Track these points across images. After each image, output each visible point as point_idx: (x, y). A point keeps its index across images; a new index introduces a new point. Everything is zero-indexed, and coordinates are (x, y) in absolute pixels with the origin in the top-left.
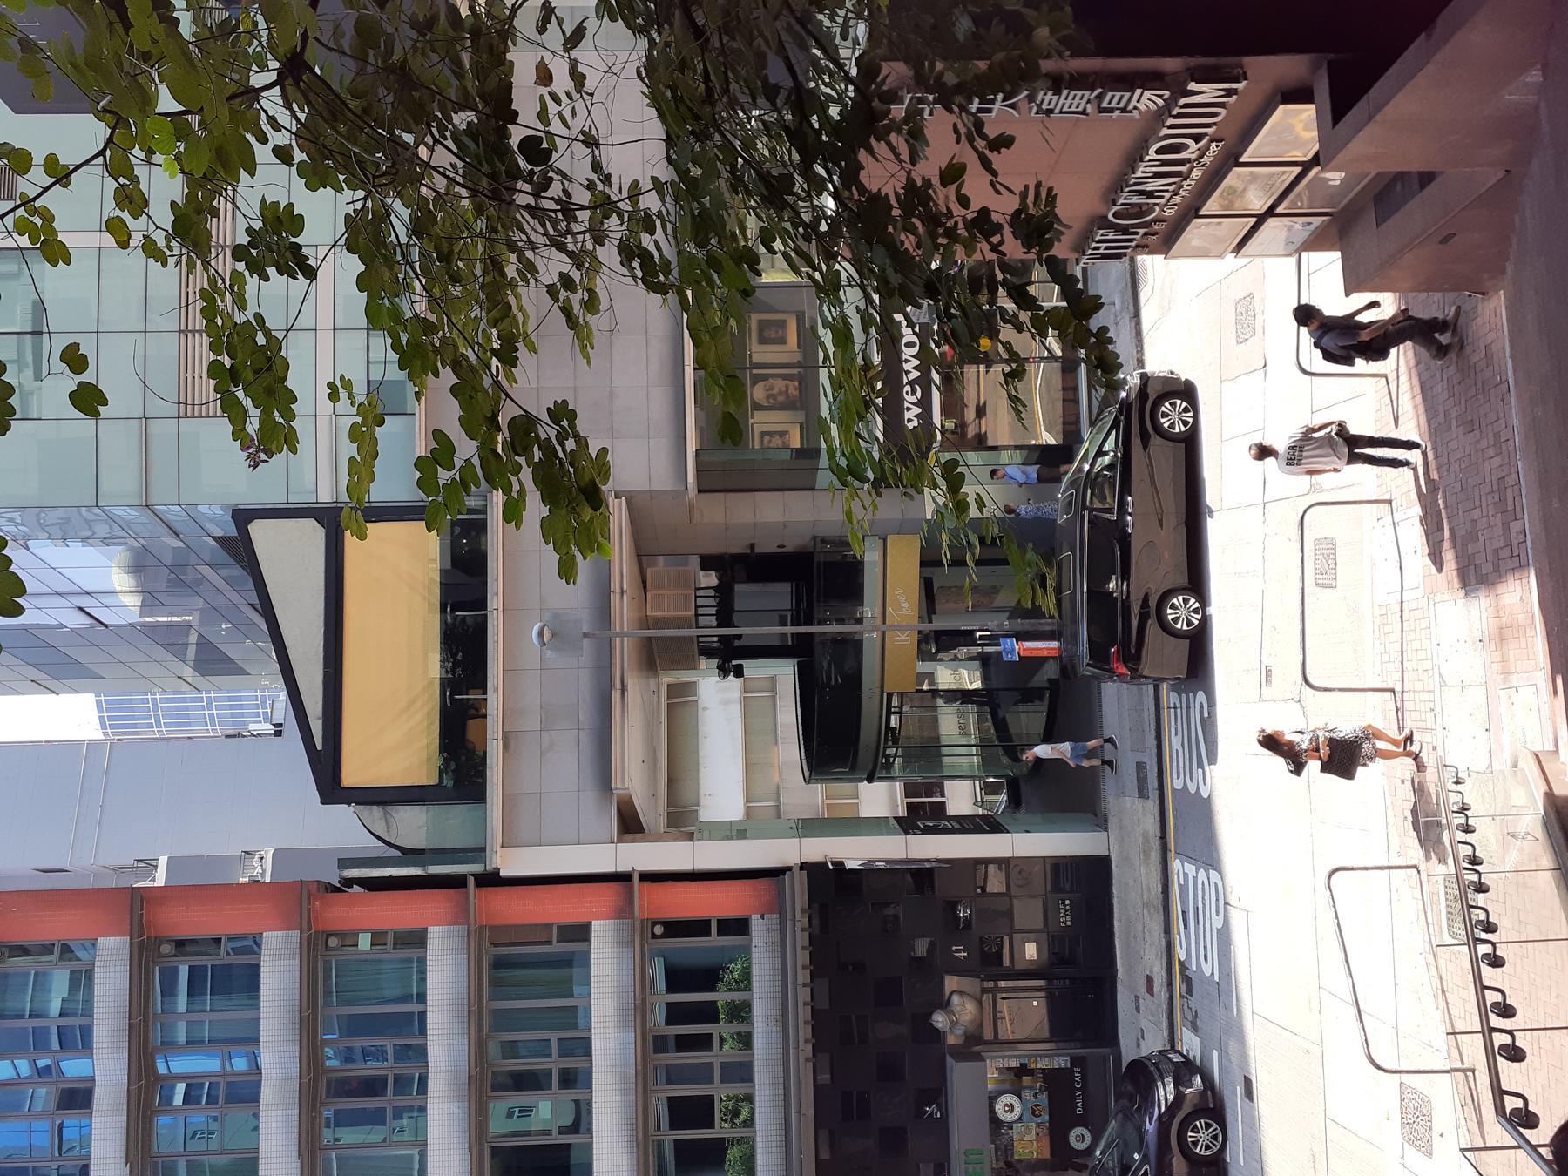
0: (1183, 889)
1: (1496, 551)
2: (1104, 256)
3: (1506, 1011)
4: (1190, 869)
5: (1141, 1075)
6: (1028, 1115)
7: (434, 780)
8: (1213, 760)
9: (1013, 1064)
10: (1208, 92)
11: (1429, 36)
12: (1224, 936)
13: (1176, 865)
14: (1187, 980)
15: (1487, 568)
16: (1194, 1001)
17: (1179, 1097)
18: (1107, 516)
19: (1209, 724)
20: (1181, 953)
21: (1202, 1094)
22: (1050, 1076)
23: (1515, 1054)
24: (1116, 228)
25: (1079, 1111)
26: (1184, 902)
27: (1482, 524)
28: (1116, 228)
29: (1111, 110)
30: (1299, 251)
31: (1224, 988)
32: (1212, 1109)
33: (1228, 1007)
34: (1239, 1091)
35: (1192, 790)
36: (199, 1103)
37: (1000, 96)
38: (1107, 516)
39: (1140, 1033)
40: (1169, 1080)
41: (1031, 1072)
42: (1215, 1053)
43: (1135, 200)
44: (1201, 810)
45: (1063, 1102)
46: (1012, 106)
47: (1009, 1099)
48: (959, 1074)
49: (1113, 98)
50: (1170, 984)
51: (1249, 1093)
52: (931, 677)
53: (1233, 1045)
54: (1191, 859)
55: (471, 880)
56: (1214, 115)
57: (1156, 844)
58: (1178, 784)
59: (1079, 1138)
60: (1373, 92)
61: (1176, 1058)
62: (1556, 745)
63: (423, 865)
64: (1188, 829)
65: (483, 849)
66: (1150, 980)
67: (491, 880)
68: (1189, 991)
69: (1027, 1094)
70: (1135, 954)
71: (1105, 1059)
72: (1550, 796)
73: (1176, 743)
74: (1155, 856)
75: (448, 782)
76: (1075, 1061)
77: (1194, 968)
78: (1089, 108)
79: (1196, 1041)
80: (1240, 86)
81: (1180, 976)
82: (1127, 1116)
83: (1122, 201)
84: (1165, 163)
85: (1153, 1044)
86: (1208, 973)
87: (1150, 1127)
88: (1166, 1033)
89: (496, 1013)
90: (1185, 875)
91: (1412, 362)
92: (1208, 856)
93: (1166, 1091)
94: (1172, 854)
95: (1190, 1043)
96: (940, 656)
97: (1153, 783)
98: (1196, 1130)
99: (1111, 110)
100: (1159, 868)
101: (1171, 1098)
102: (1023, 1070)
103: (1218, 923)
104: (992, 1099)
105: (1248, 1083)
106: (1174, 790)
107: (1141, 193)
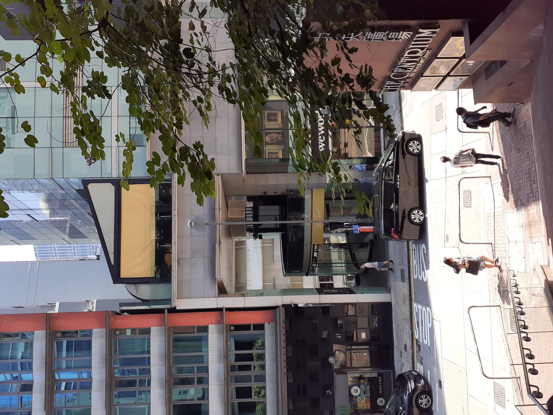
0: (417, 314)
1: (528, 194)
2: (389, 91)
3: (531, 357)
4: (420, 307)
5: (402, 379)
6: (362, 393)
7: (153, 275)
8: (428, 268)
9: (357, 375)
10: (426, 32)
11: (504, 13)
12: (432, 330)
13: (415, 305)
14: (419, 346)
15: (524, 200)
16: (421, 353)
17: (416, 387)
18: (390, 182)
19: (426, 256)
20: (416, 336)
21: (424, 386)
22: (370, 380)
23: (534, 372)
24: (394, 80)
25: (381, 392)
26: (418, 318)
27: (522, 185)
28: (394, 80)
29: (392, 39)
30: (458, 89)
31: (432, 349)
32: (428, 391)
33: (433, 355)
34: (437, 385)
35: (420, 279)
36: (70, 389)
37: (353, 34)
38: (390, 182)
39: (402, 365)
40: (412, 381)
41: (364, 378)
42: (429, 372)
43: (400, 71)
44: (424, 286)
45: (375, 389)
46: (357, 37)
47: (356, 388)
48: (338, 379)
49: (393, 35)
50: (413, 347)
51: (440, 386)
52: (328, 239)
53: (435, 369)
54: (420, 303)
55: (166, 311)
56: (428, 40)
57: (408, 298)
58: (416, 277)
59: (380, 402)
60: (484, 33)
61: (415, 373)
62: (549, 263)
63: (149, 305)
64: (419, 293)
65: (170, 300)
66: (405, 346)
67: (173, 310)
68: (419, 350)
69: (362, 386)
70: (400, 337)
71: (390, 374)
72: (547, 281)
73: (415, 262)
74: (407, 302)
75: (158, 276)
76: (379, 374)
77: (421, 341)
78: (384, 38)
79: (422, 367)
80: (437, 30)
81: (416, 345)
82: (398, 394)
83: (396, 71)
84: (411, 58)
85: (407, 368)
86: (426, 343)
87: (406, 398)
88: (411, 365)
89: (175, 357)
90: (418, 309)
91: (498, 128)
92: (426, 302)
93: (411, 385)
94: (413, 302)
95: (420, 368)
96: (332, 231)
97: (406, 276)
98: (422, 399)
99: (392, 39)
100: (409, 306)
101: (413, 387)
102: (361, 378)
103: (429, 326)
104: (350, 388)
105: (440, 382)
106: (414, 279)
107: (402, 68)
